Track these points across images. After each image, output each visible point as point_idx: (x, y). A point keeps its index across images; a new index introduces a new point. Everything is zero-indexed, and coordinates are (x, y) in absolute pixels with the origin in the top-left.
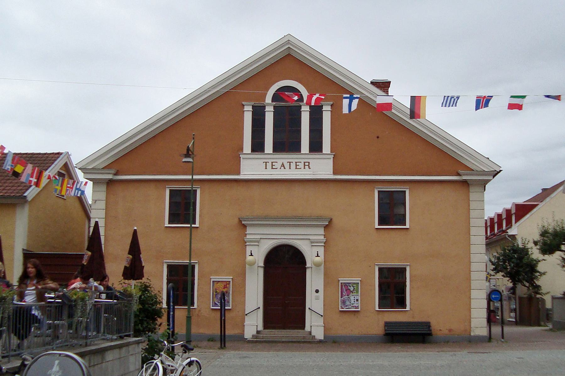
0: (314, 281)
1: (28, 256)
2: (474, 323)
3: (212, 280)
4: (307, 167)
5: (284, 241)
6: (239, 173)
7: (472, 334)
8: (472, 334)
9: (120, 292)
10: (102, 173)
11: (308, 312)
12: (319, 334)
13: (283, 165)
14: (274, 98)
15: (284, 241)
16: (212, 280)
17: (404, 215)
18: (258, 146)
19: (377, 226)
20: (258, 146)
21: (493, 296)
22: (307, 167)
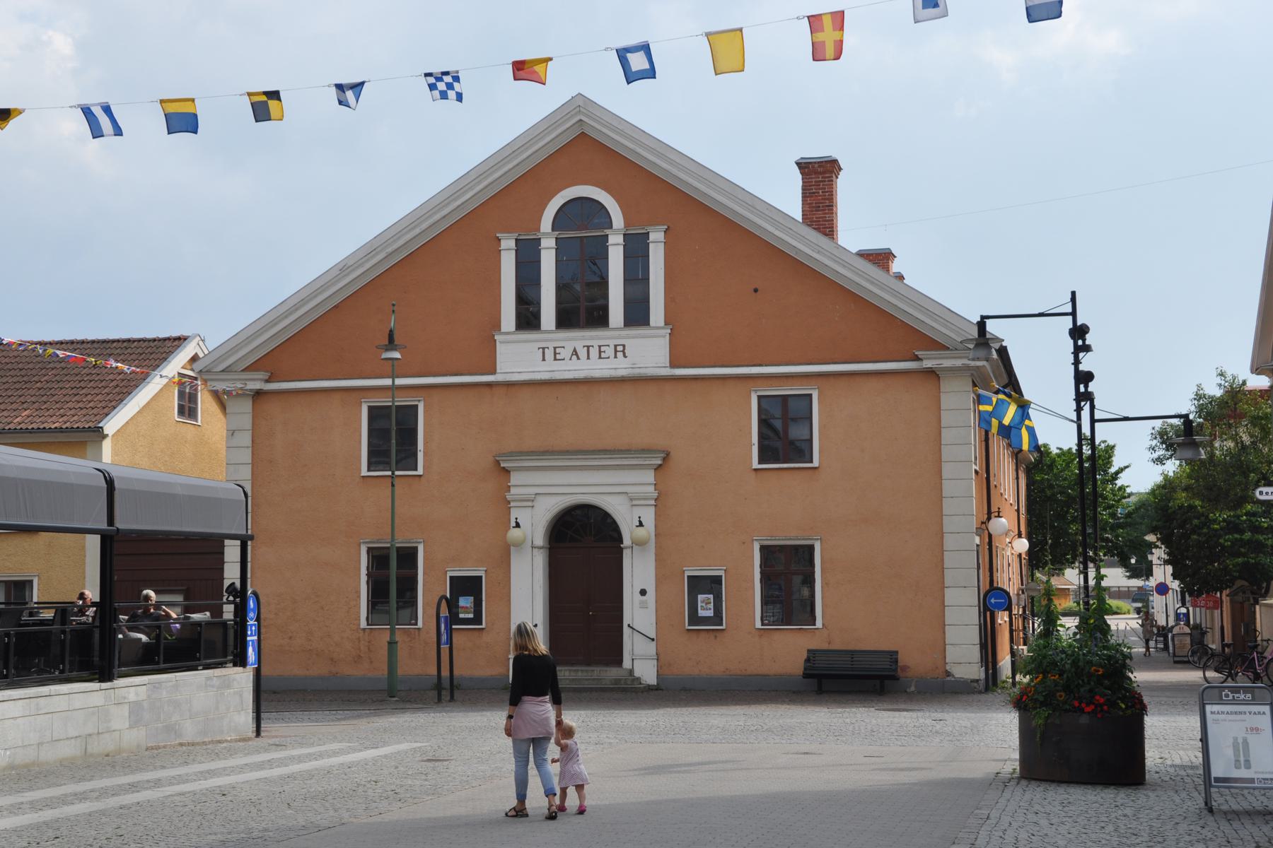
4: (620, 355)
6: (494, 372)
11: (626, 630)
14: (555, 226)
18: (528, 319)
20: (528, 319)
22: (620, 355)
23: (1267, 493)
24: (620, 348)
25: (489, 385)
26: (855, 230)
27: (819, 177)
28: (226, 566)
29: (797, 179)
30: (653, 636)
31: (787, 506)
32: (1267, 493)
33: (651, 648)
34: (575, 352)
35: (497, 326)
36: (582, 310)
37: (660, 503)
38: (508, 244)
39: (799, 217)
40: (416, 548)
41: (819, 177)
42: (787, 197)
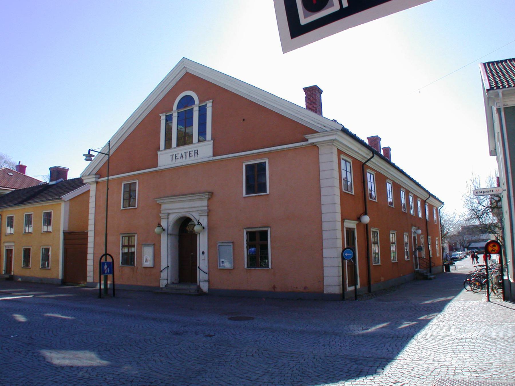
0: (202, 243)
1: (65, 233)
2: (327, 281)
3: (218, 244)
4: (196, 154)
5: (183, 213)
6: (157, 167)
7: (325, 292)
8: (325, 292)
9: (456, 259)
10: (331, 135)
11: (198, 269)
12: (205, 287)
13: (182, 156)
14: (178, 108)
15: (183, 213)
16: (218, 244)
17: (265, 184)
18: (168, 145)
19: (122, 208)
20: (168, 145)
21: (346, 254)
22: (196, 154)
23: (314, 2)
24: (196, 152)
25: (156, 171)
26: (331, 109)
27: (313, 95)
28: (89, 244)
29: (303, 95)
30: (207, 271)
31: (255, 211)
32: (314, 2)
33: (206, 277)
34: (182, 156)
35: (158, 149)
36: (184, 139)
37: (209, 213)
38: (163, 118)
39: (303, 104)
40: (247, 193)
41: (313, 95)
42: (301, 100)
